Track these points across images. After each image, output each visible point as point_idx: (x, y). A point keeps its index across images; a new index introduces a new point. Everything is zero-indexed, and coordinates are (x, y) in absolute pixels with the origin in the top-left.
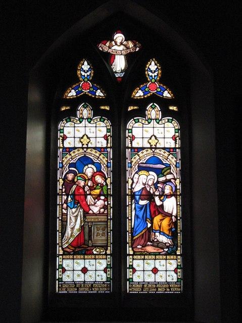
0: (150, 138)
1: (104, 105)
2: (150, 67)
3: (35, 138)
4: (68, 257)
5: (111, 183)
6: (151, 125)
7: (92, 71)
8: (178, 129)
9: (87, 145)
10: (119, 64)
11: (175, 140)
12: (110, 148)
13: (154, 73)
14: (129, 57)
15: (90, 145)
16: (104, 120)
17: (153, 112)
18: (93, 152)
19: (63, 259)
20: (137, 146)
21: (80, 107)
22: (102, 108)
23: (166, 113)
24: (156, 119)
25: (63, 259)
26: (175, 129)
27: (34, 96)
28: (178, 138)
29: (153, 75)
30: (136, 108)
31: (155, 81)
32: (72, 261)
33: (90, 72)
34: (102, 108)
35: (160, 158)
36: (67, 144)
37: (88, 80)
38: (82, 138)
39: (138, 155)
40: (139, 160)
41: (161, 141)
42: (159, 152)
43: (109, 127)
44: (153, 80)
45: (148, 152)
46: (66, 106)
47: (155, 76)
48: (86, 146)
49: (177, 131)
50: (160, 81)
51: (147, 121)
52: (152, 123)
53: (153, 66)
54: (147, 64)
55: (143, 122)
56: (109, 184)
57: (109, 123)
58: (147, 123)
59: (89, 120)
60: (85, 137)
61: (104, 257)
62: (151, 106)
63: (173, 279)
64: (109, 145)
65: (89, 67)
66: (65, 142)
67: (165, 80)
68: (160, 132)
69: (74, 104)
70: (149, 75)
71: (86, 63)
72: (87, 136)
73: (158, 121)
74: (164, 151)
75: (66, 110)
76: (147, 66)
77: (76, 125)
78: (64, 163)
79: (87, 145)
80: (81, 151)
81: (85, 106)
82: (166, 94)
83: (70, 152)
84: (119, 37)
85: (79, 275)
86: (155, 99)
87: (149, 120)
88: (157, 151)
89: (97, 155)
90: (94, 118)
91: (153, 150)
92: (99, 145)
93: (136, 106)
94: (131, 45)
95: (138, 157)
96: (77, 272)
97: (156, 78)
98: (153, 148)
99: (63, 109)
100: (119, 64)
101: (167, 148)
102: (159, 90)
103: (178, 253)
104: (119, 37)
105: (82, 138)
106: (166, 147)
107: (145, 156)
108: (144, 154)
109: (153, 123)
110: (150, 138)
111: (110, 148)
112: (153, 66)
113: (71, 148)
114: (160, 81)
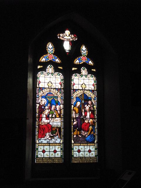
0: (48, 83)
1: (93, 69)
2: (83, 48)
3: (30, 81)
4: (76, 144)
5: (96, 108)
6: (49, 76)
7: (54, 49)
8: (63, 79)
9: (85, 88)
10: (67, 46)
11: (61, 85)
12: (96, 90)
13: (85, 51)
14: (72, 43)
15: (86, 89)
16: (93, 76)
17: (84, 71)
18: (88, 92)
19: (38, 146)
20: (76, 88)
21: (48, 67)
22: (92, 70)
23: (90, 72)
24: (85, 75)
25: (38, 146)
26: (61, 79)
27: (30, 60)
28: (62, 84)
29: (84, 52)
30: (41, 67)
31: (52, 53)
32: (83, 146)
33: (86, 51)
34: (92, 70)
35: (87, 95)
36: (41, 86)
37: (52, 53)
38: (82, 85)
39: (42, 91)
40: (42, 94)
41: (87, 86)
42: (87, 92)
43: (95, 80)
44: (51, 53)
45: (81, 91)
46: (40, 66)
47: (85, 53)
48: (50, 87)
49: (62, 80)
50: (54, 54)
51: (47, 74)
52: (83, 77)
53: (84, 48)
54: (81, 47)
55: (45, 74)
56: (95, 108)
57: (62, 77)
58: (47, 75)
59: (86, 76)
60: (50, 83)
61: (59, 144)
62: (49, 66)
63: (41, 156)
64: (62, 88)
65: (85, 49)
66: (40, 85)
67: (89, 56)
68: (54, 80)
69: (79, 67)
70: (48, 50)
71: (84, 46)
72: (84, 84)
73: (86, 76)
74: (89, 91)
75: (74, 70)
76: (81, 48)
77: (46, 76)
78: (74, 97)
79: (85, 88)
80: (48, 90)
81: (51, 67)
82: (57, 60)
83: (42, 90)
84: (67, 32)
85: (92, 154)
86: (52, 63)
87: (82, 76)
88: (86, 91)
89: (90, 94)
90: (55, 73)
91: (84, 91)
92: (57, 87)
93: (76, 68)
94: (73, 36)
95: (42, 92)
96: (47, 151)
97: (85, 54)
98: (84, 90)
99: (38, 68)
100: (67, 46)
101: (57, 89)
102: (87, 60)
103: (96, 142)
104: (67, 32)
105: (82, 85)
106: (56, 88)
107: (46, 91)
108: (45, 91)
109: (50, 75)
110: (48, 83)
111: (96, 90)
112: (84, 48)
113: (43, 88)
114: (54, 54)
